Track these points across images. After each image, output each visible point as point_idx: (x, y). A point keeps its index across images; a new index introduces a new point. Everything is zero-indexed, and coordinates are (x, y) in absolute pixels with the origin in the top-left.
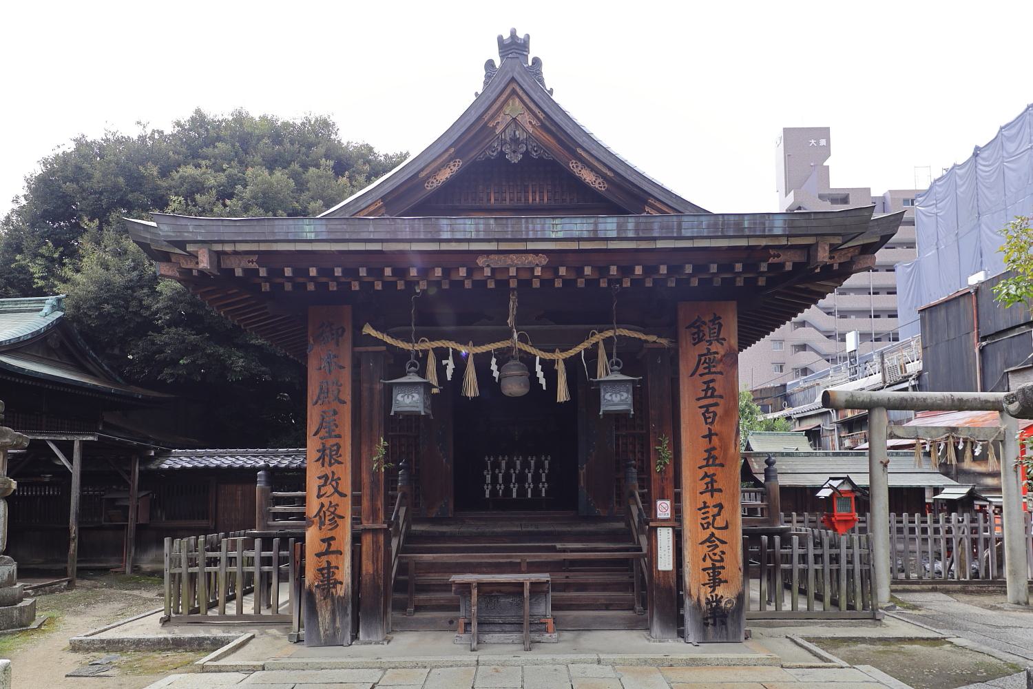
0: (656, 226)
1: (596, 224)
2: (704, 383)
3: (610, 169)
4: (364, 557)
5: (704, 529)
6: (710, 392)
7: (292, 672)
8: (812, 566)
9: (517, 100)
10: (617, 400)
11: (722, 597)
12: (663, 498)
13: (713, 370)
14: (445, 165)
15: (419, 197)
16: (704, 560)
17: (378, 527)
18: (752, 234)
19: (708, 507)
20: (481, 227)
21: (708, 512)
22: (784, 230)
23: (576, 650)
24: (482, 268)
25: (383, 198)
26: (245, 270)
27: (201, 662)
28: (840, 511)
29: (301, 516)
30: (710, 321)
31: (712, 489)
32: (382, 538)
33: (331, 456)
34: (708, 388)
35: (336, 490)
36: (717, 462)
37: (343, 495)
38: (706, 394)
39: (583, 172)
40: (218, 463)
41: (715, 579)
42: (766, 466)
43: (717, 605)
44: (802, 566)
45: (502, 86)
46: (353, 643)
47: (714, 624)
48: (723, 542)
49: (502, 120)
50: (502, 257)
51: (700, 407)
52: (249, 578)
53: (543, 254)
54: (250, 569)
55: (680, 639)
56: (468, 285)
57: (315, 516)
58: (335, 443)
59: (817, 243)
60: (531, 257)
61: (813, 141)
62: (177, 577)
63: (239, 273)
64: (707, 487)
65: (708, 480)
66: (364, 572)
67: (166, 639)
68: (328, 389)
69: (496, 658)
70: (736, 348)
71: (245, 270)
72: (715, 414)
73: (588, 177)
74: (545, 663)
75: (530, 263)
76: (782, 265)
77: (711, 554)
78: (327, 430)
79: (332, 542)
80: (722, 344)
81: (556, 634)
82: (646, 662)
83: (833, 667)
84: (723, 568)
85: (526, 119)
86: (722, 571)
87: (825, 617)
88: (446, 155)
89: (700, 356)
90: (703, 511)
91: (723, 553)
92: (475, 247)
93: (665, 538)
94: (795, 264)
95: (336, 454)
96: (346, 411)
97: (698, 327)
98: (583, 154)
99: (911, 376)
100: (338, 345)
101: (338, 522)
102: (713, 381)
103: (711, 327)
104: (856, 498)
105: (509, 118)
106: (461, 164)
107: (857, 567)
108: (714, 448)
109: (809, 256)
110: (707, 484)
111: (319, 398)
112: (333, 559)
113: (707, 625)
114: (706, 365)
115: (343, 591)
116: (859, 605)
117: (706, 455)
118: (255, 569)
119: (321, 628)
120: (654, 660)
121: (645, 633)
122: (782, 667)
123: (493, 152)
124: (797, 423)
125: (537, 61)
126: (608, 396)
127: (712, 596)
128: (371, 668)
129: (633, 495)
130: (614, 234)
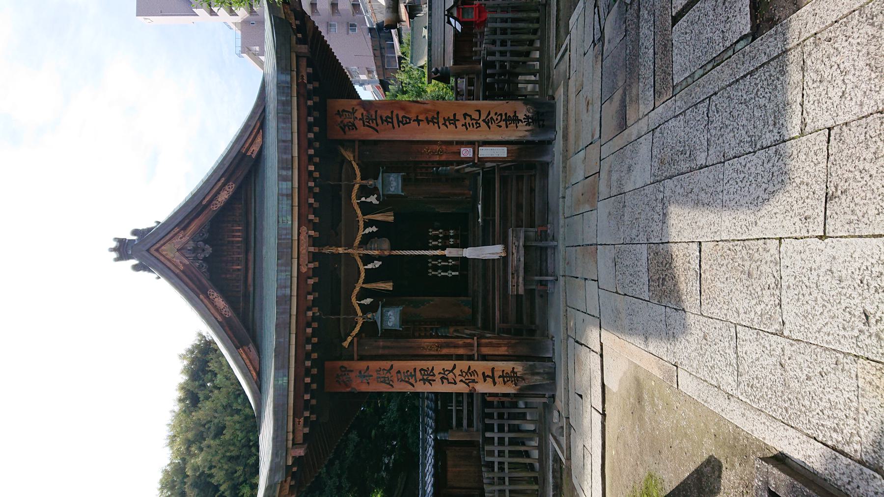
3: (219, 180)
4: (497, 353)
8: (509, 48)
9: (163, 248)
10: (394, 184)
12: (459, 153)
14: (212, 302)
15: (236, 321)
16: (500, 126)
25: (238, 348)
26: (305, 425)
28: (471, 16)
29: (471, 395)
31: (454, 121)
32: (484, 341)
33: (428, 375)
34: (386, 121)
35: (452, 371)
41: (516, 120)
44: (508, 54)
45: (153, 259)
47: (543, 121)
48: (489, 114)
49: (181, 261)
52: (512, 442)
54: (507, 440)
60: (302, 237)
63: (307, 430)
65: (447, 123)
71: (305, 425)
72: (404, 117)
73: (224, 197)
76: (308, 75)
82: (565, 167)
84: (506, 114)
85: (179, 241)
87: (544, 40)
89: (364, 125)
91: (496, 114)
92: (295, 274)
93: (485, 152)
94: (308, 66)
96: (398, 364)
97: (345, 126)
100: (352, 371)
102: (381, 117)
104: (462, 4)
107: (509, 15)
108: (427, 119)
111: (388, 384)
112: (497, 374)
113: (543, 125)
117: (431, 124)
125: (135, 232)
126: (392, 189)
129: (458, 171)
130: (290, 183)
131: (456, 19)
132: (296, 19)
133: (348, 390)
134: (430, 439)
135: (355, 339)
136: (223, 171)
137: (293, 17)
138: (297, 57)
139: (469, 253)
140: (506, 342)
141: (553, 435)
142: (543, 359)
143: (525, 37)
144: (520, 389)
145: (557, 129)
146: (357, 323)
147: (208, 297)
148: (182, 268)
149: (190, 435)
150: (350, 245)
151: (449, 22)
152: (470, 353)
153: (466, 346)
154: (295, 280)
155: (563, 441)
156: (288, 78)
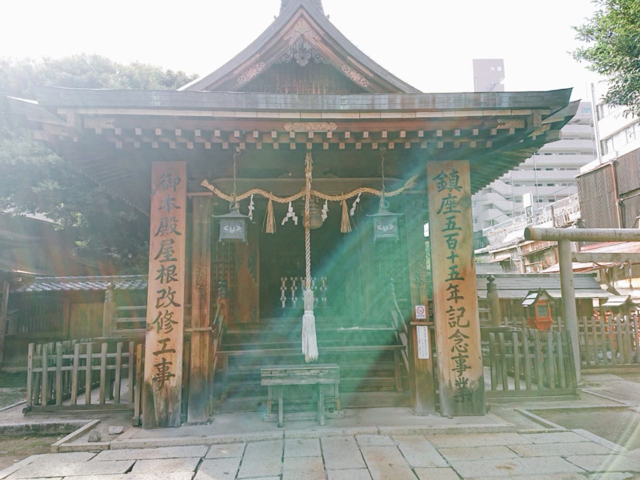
0: (417, 101)
1: (373, 100)
2: (448, 219)
3: (371, 71)
4: (193, 354)
5: (451, 327)
6: (452, 225)
7: (133, 450)
8: (529, 356)
9: (304, 22)
11: (467, 380)
13: (453, 209)
14: (251, 66)
16: (453, 350)
17: (204, 330)
18: (486, 107)
19: (454, 310)
20: (289, 101)
21: (454, 314)
22: (510, 105)
23: (358, 424)
24: (289, 133)
27: (57, 444)
28: (540, 315)
29: (143, 325)
30: (450, 174)
33: (169, 275)
34: (450, 222)
35: (172, 302)
36: (459, 277)
37: (177, 305)
38: (449, 226)
39: (352, 73)
40: (72, 287)
41: (462, 368)
42: (488, 282)
43: (464, 385)
46: (183, 424)
47: (463, 401)
48: (466, 337)
49: (293, 37)
50: (303, 124)
51: (445, 236)
53: (333, 122)
54: (97, 368)
55: (437, 413)
56: (276, 146)
57: (154, 323)
58: (171, 265)
59: (533, 114)
60: (324, 125)
61: (492, 68)
62: (38, 376)
64: (453, 295)
65: (452, 290)
66: (192, 366)
67: (27, 426)
68: (167, 224)
69: (299, 432)
70: (469, 192)
72: (456, 241)
74: (337, 434)
75: (323, 129)
76: (507, 130)
77: (457, 346)
78: (166, 255)
79: (167, 343)
80: (460, 191)
81: (343, 411)
82: (415, 432)
83: (556, 431)
84: (467, 357)
85: (310, 35)
86: (466, 359)
88: (254, 59)
90: (450, 313)
91: (466, 345)
95: (173, 273)
97: (441, 179)
98: (353, 61)
99: (573, 222)
101: (172, 327)
102: (454, 217)
103: (451, 178)
105: (298, 34)
106: (264, 66)
108: (456, 266)
109: (526, 124)
110: (452, 293)
111: (159, 231)
112: (168, 356)
113: (457, 401)
114: (448, 206)
115: (175, 382)
116: (563, 384)
117: (450, 271)
118: (102, 368)
119: (156, 414)
120: (421, 430)
121: (409, 409)
122: (518, 433)
123: (287, 58)
124: (493, 257)
127: (460, 379)
128: (198, 445)
130: (386, 107)
131: (536, 299)
132: (537, 136)
133: (154, 187)
134: (106, 285)
135: (211, 194)
136: (380, 74)
137: (538, 134)
138: (525, 118)
139: (309, 317)
140: (206, 365)
141: (97, 424)
142: (184, 410)
143: (541, 372)
144: (148, 385)
145: (456, 419)
146: (229, 195)
147: (257, 62)
148: (286, 38)
149: (136, 76)
150: (314, 187)
151: (530, 293)
152: (193, 323)
153: (202, 316)
154: (275, 116)
155: (82, 442)
156: (505, 105)
